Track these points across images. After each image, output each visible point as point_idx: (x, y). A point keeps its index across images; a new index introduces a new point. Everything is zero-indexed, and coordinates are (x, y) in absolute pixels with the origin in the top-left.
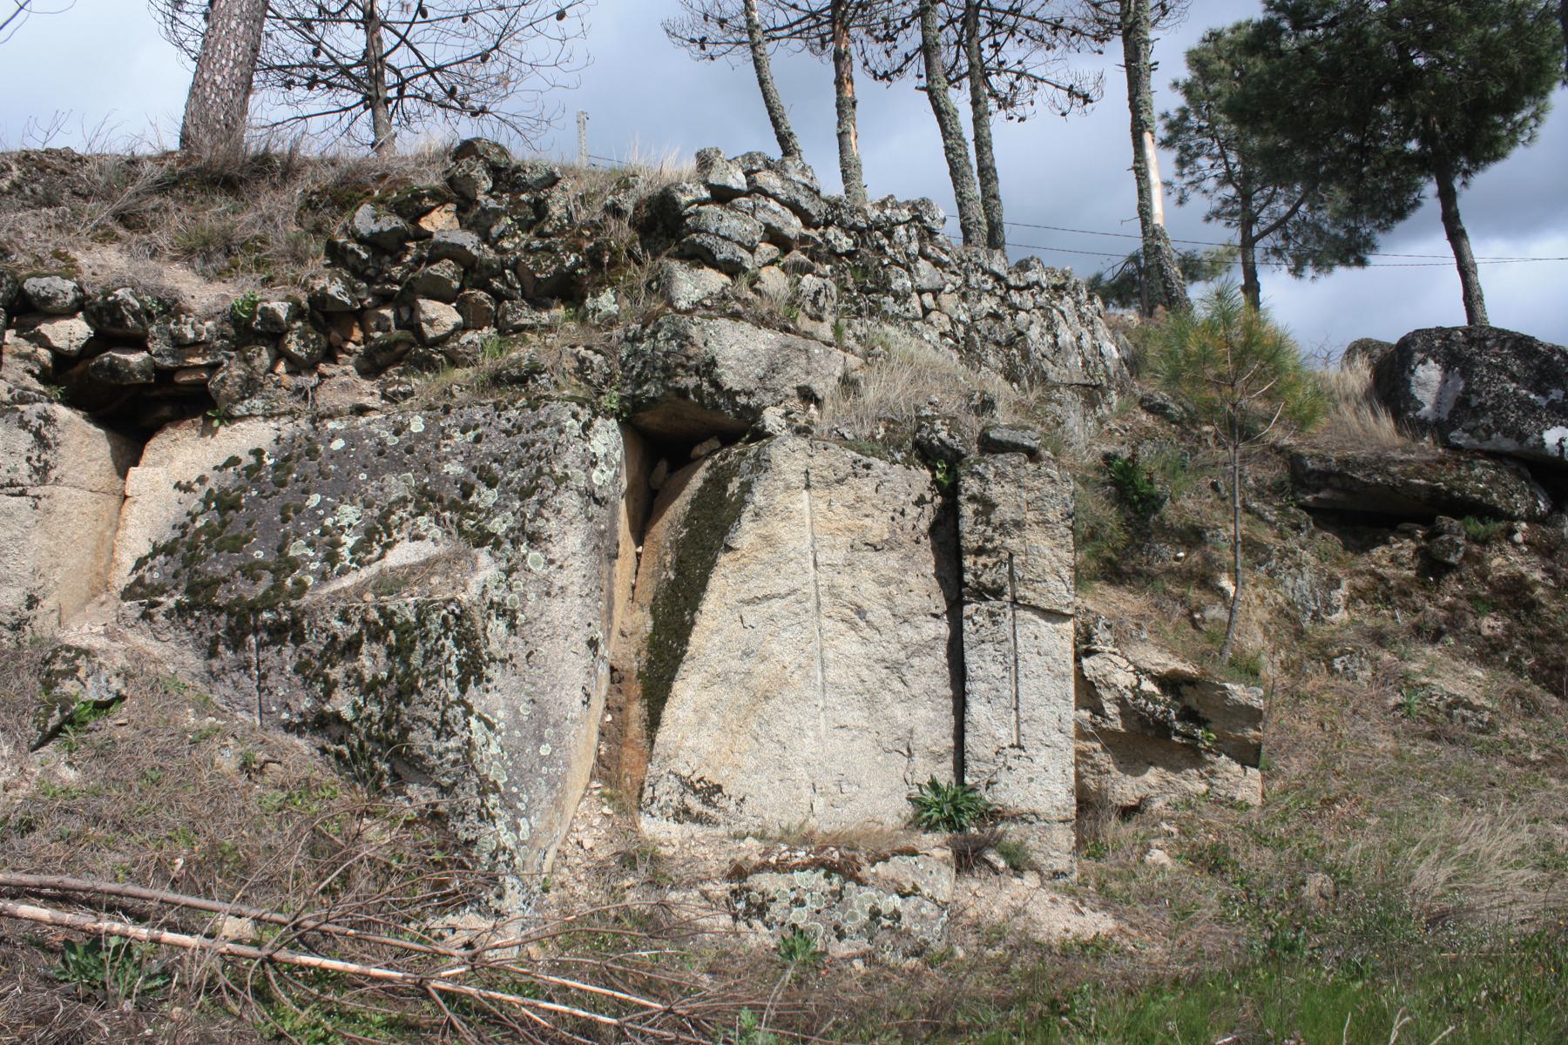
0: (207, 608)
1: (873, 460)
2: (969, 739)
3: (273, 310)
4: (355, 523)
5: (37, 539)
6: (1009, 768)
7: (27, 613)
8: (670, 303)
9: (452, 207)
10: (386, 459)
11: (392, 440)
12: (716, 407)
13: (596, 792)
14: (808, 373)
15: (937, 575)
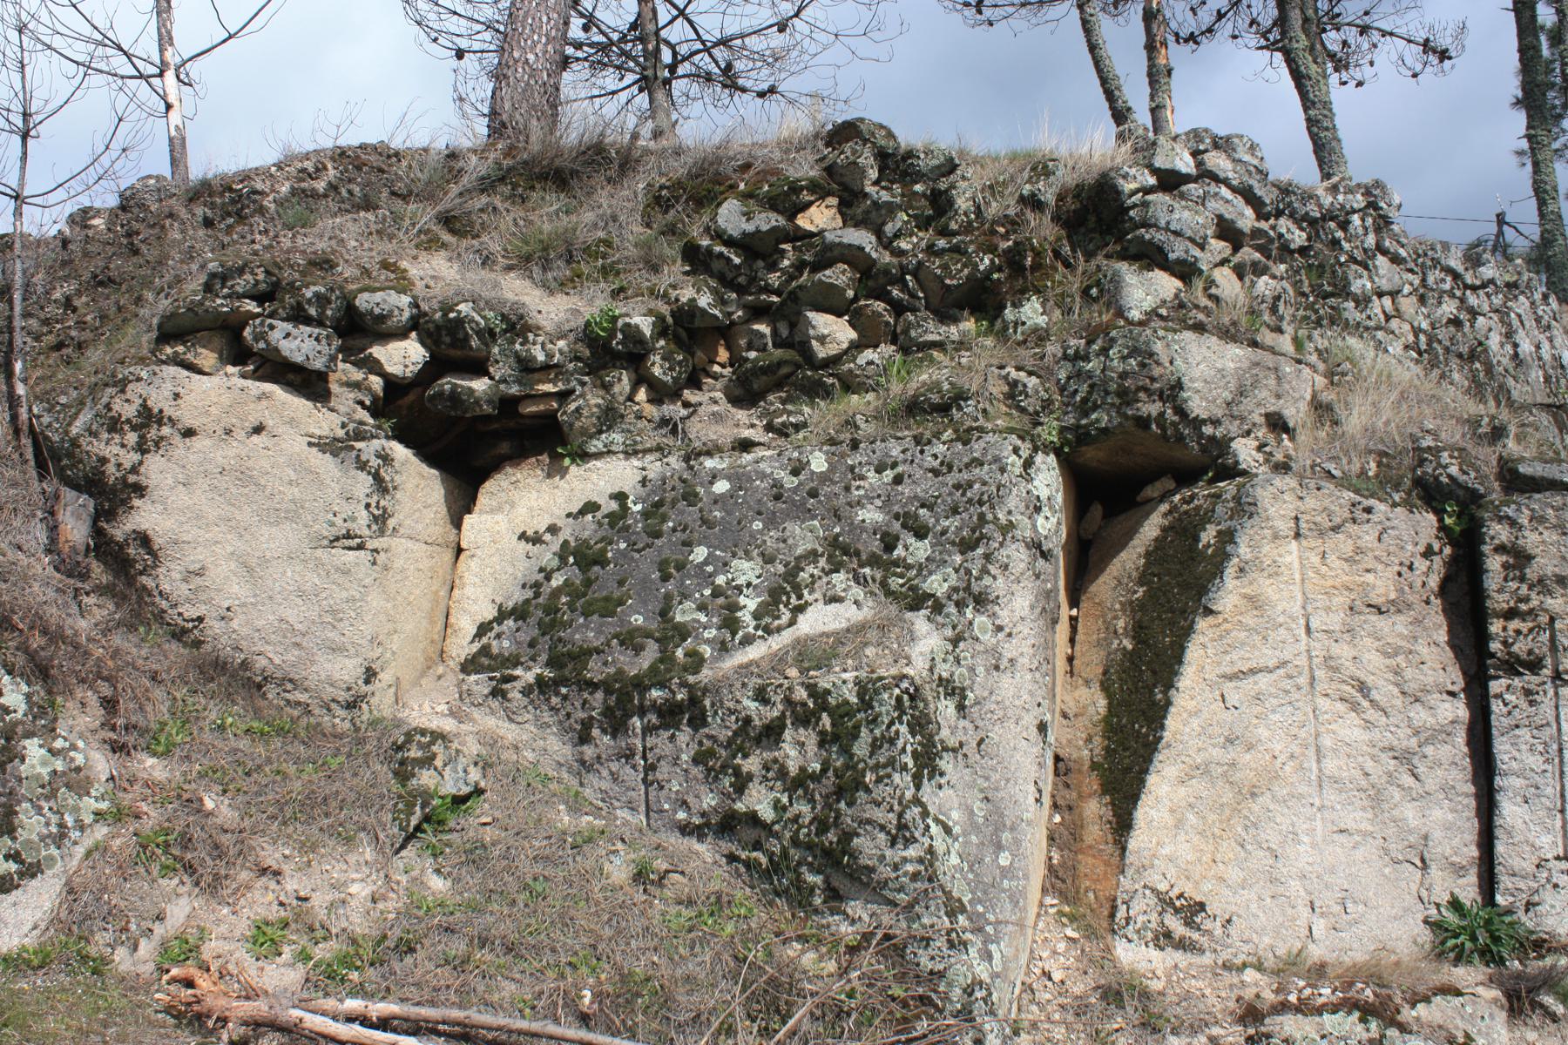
0: (578, 683)
1: (1372, 502)
2: (1500, 848)
3: (637, 326)
4: (756, 582)
5: (375, 601)
6: (1556, 886)
7: (365, 689)
8: (1120, 313)
9: (833, 201)
10: (783, 504)
11: (790, 482)
12: (1180, 438)
13: (1052, 911)
14: (1278, 397)
15: (1452, 644)
